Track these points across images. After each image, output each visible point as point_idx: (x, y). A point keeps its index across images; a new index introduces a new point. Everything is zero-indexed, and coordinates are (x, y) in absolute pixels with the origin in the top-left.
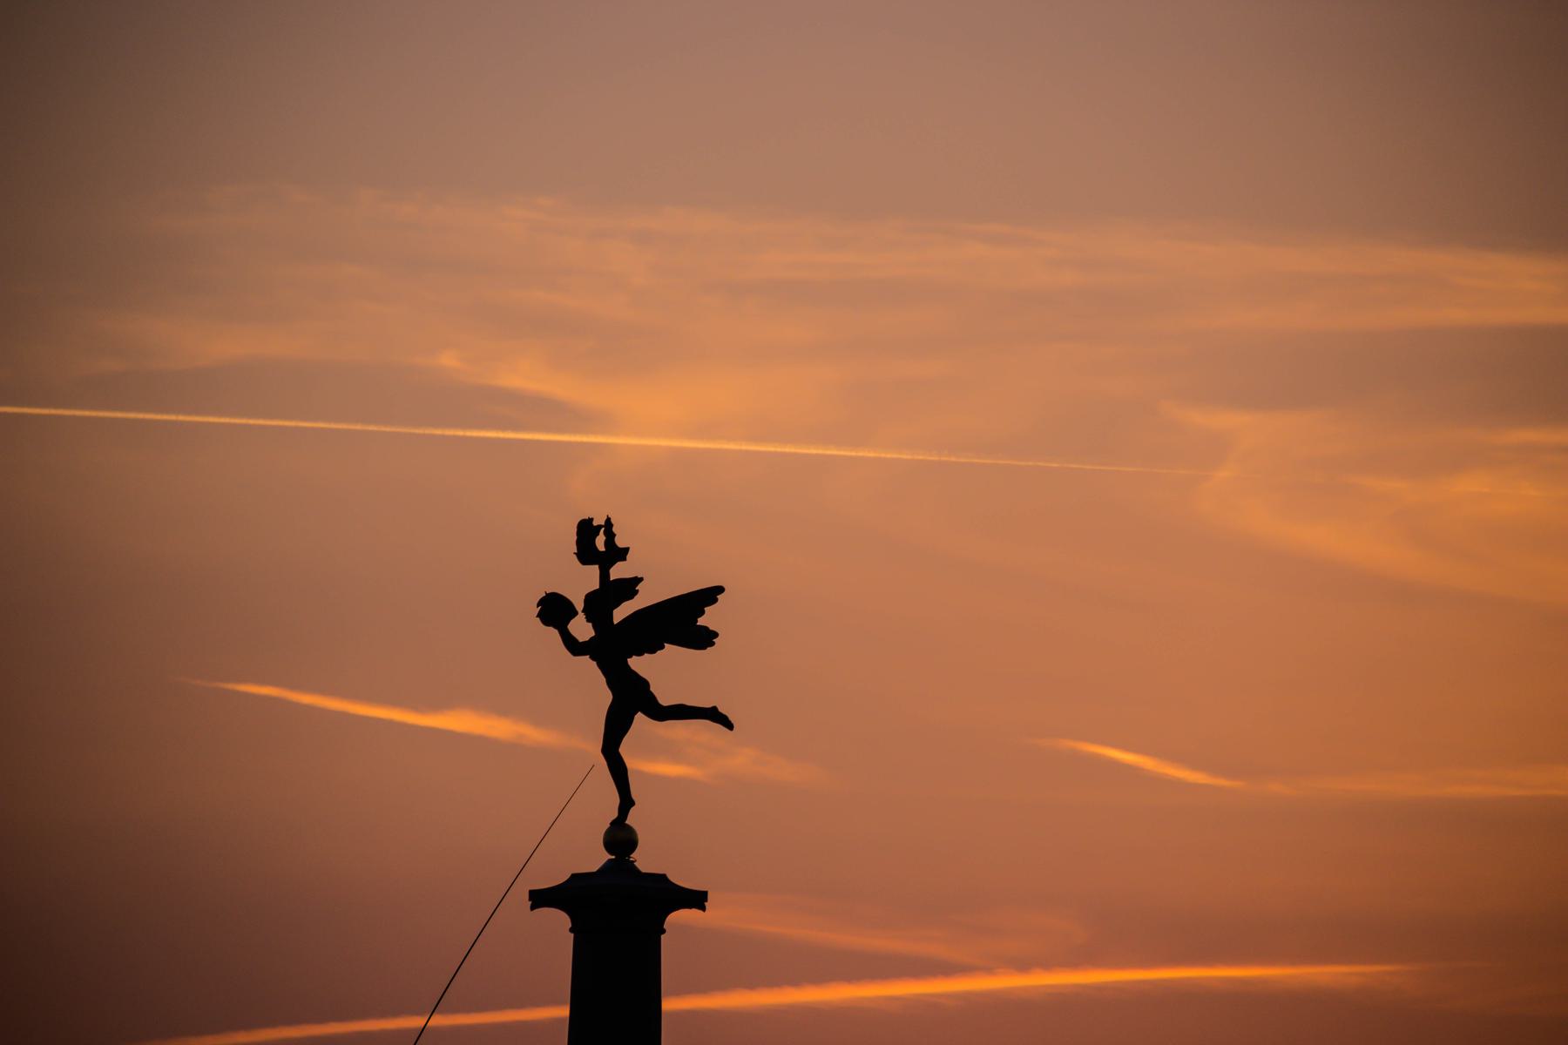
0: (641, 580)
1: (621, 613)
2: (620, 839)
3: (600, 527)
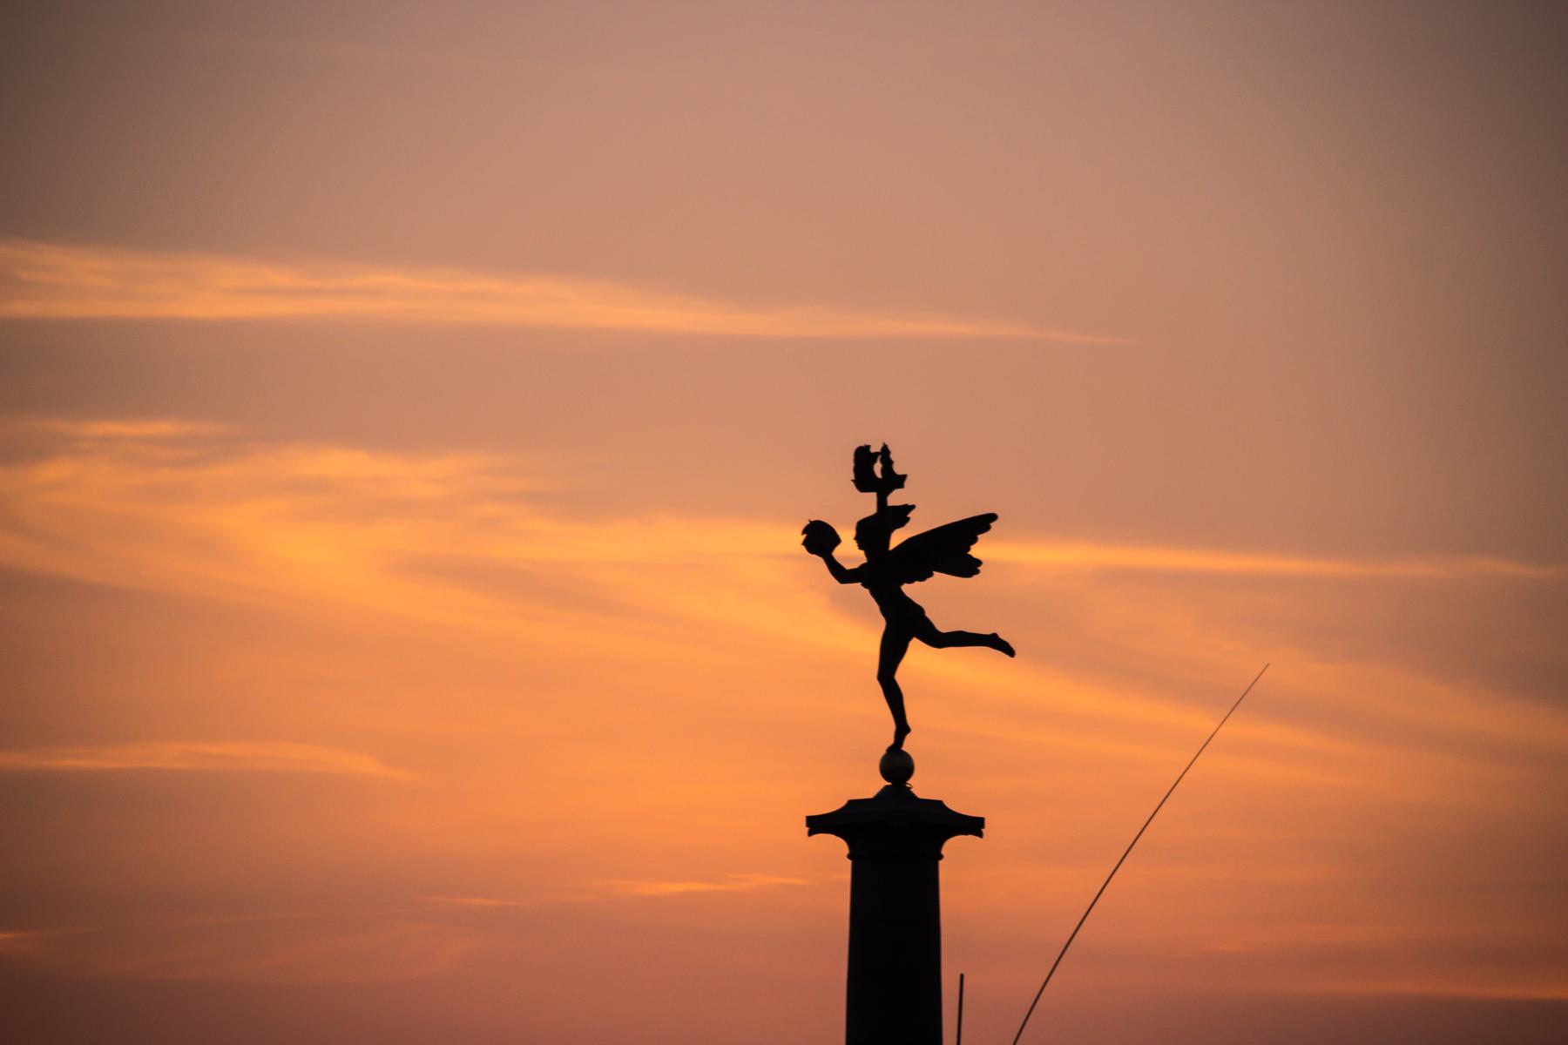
0: (913, 507)
1: (897, 538)
2: (897, 765)
3: (877, 454)
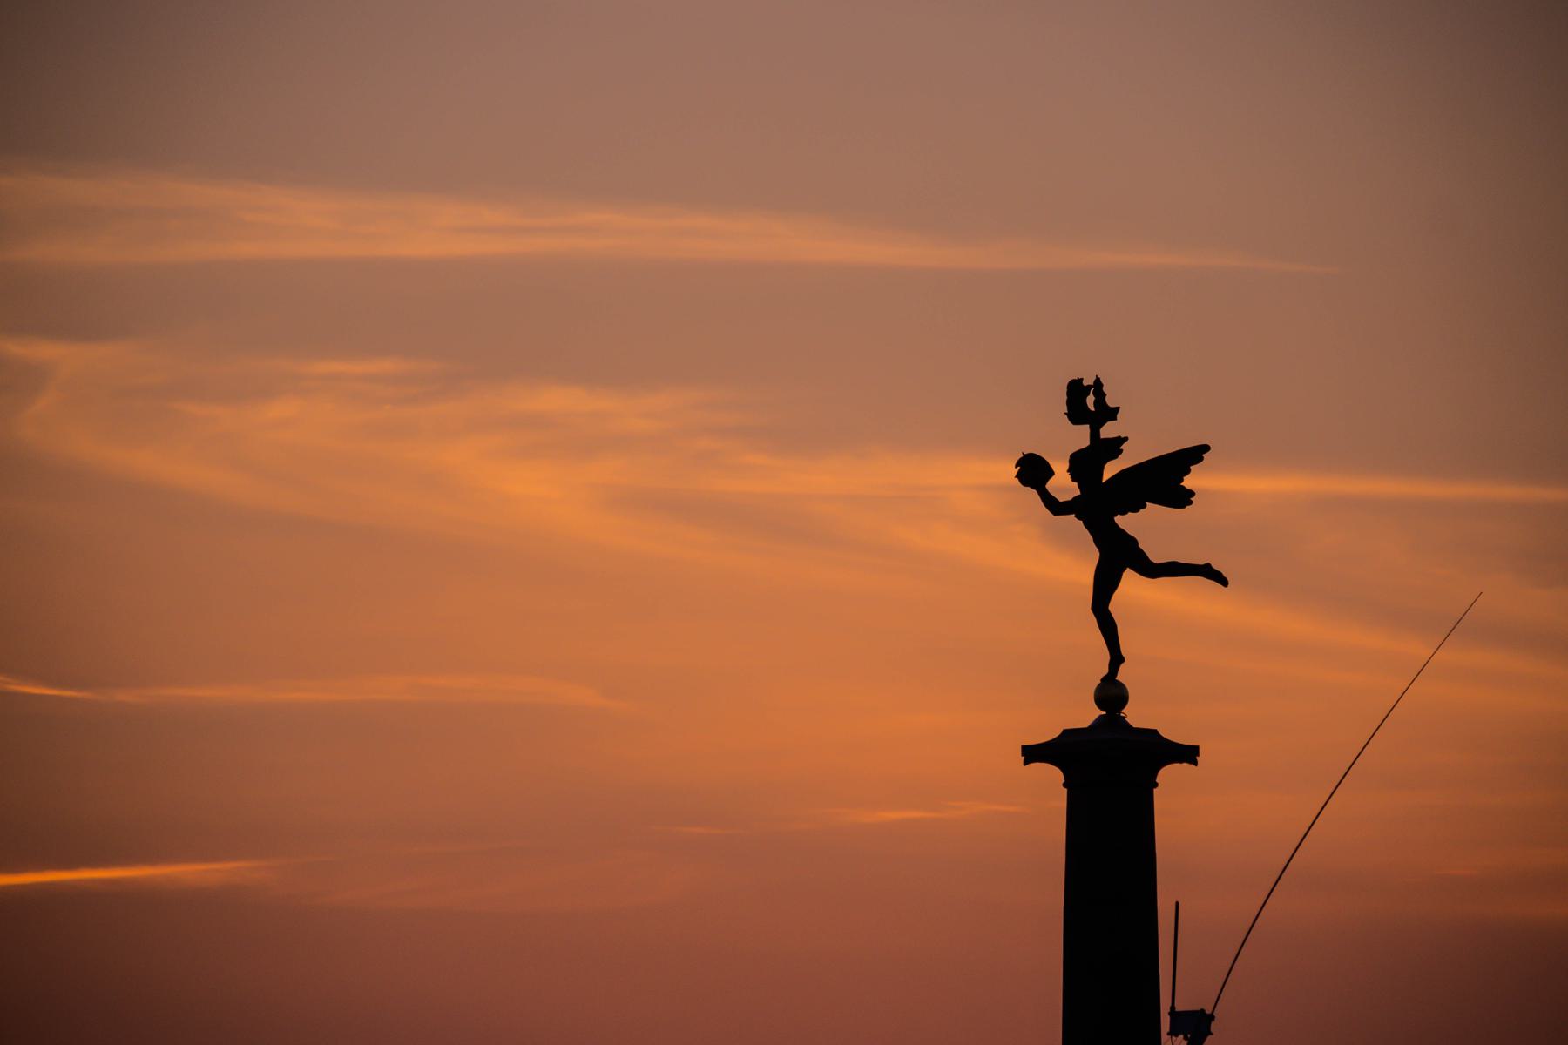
0: (1126, 439)
1: (1110, 470)
2: (1111, 694)
3: (1089, 387)
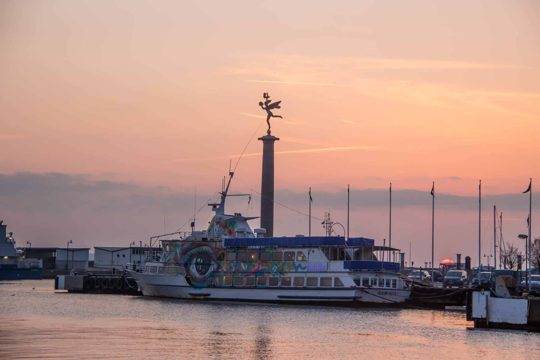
1: (269, 104)
2: (269, 132)
